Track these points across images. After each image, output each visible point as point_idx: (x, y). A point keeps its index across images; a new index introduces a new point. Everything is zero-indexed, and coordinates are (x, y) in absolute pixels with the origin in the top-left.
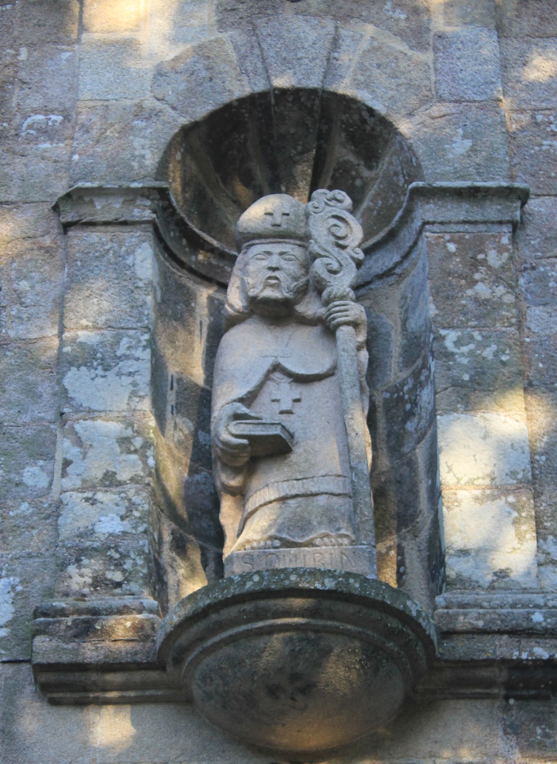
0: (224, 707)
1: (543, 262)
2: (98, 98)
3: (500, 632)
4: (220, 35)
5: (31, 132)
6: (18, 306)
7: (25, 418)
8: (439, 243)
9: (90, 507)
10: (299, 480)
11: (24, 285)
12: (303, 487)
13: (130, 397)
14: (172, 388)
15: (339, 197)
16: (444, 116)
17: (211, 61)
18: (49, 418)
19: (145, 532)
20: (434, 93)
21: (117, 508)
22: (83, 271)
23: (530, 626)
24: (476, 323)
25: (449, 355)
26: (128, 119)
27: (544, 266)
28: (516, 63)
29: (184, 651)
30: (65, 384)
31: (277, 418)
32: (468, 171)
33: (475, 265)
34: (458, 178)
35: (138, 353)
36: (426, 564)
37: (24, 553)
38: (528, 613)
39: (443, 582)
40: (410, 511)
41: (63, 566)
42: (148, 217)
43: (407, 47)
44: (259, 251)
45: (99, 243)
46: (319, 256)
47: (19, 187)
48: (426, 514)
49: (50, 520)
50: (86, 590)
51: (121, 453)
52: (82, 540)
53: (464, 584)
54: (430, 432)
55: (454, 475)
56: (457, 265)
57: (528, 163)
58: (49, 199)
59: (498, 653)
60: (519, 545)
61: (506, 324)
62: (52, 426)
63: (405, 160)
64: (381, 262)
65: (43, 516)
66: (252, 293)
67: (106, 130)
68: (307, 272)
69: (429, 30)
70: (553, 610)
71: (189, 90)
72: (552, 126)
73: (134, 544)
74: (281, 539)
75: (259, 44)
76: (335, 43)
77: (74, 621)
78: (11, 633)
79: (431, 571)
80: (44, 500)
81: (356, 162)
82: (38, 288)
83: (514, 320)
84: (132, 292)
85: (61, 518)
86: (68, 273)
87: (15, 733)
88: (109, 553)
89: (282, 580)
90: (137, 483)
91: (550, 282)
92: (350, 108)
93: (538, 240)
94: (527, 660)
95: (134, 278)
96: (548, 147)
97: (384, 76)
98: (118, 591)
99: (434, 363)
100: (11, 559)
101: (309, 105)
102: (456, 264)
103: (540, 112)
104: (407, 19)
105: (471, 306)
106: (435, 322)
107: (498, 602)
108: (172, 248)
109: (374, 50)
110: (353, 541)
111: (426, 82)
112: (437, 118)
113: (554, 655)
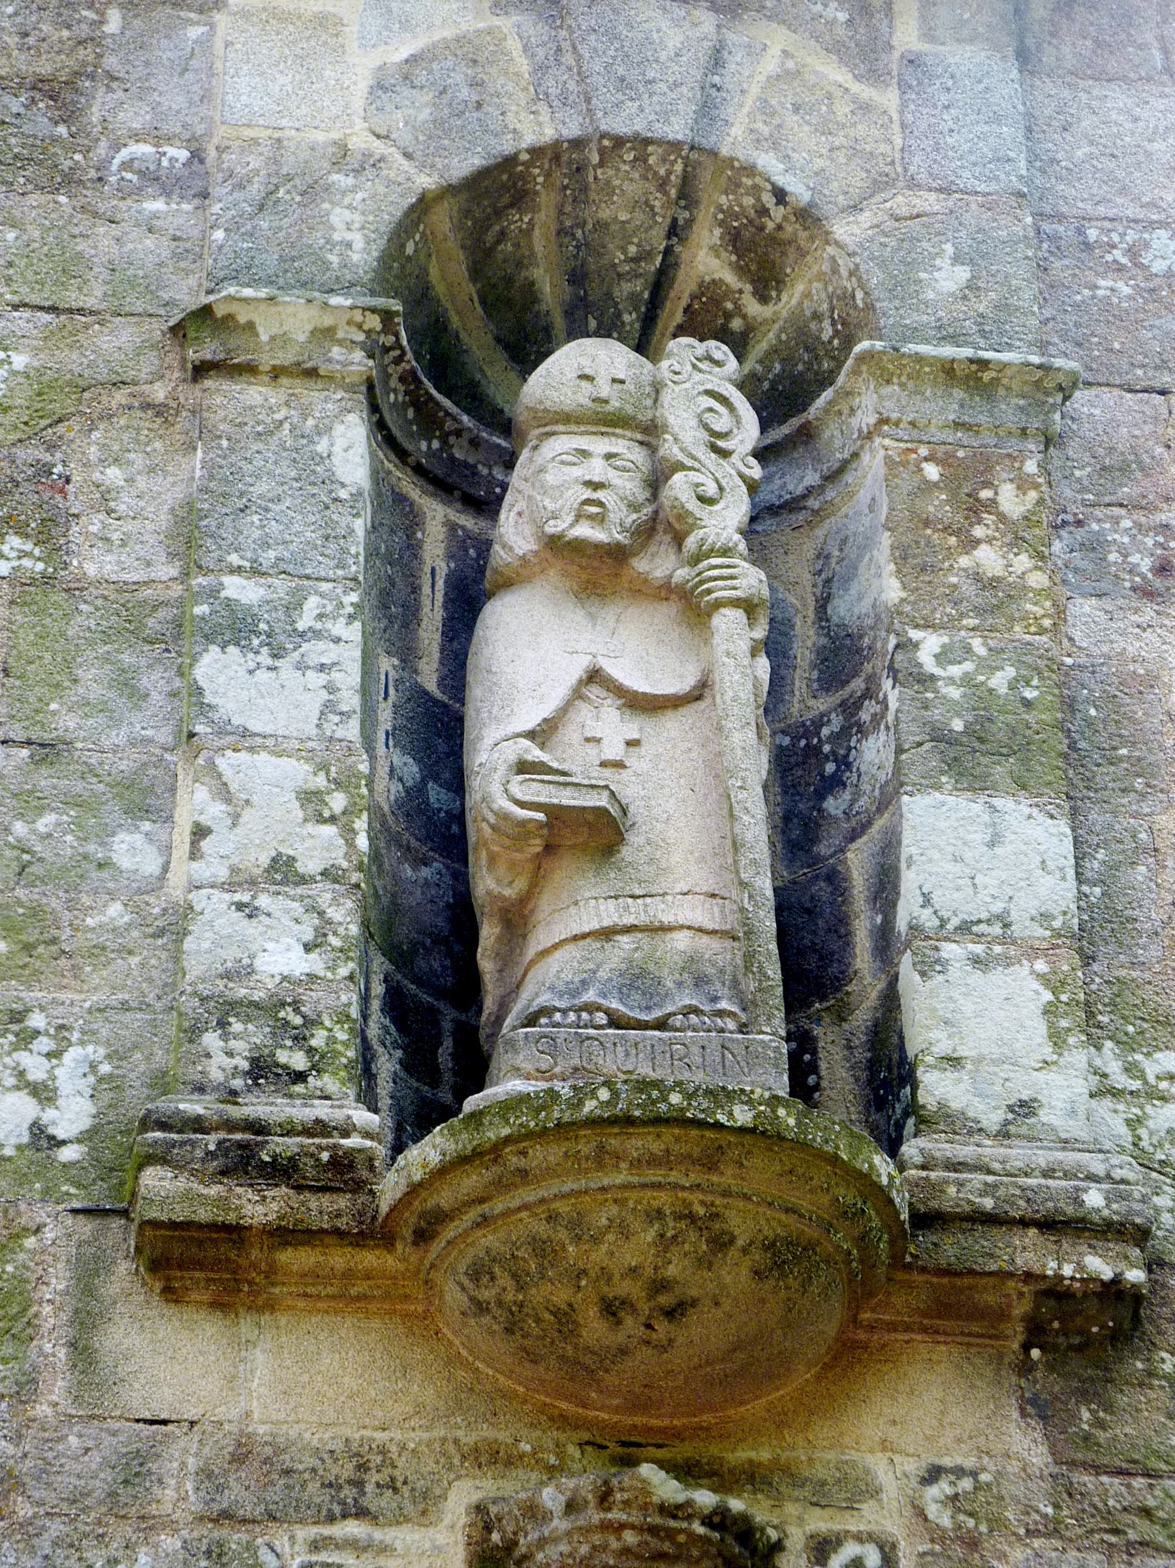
0: (508, 1331)
1: (1098, 512)
2: (261, 122)
3: (1024, 1223)
4: (497, 21)
5: (128, 176)
6: (102, 516)
7: (118, 737)
8: (908, 462)
9: (246, 922)
10: (639, 897)
11: (114, 475)
12: (646, 912)
13: (322, 713)
14: (385, 699)
15: (718, 355)
16: (918, 216)
17: (480, 69)
18: (163, 740)
19: (351, 977)
20: (899, 169)
21: (298, 926)
22: (233, 458)
23: (1080, 1215)
24: (977, 621)
25: (926, 680)
26: (320, 169)
27: (1099, 521)
28: (1049, 125)
29: (439, 1218)
30: (198, 678)
31: (595, 774)
32: (963, 327)
33: (975, 509)
34: (944, 338)
35: (338, 628)
36: (864, 1076)
37: (114, 1000)
38: (1077, 1189)
39: (906, 1114)
40: (833, 969)
41: (193, 1032)
42: (359, 364)
43: (850, 75)
44: (566, 448)
45: (262, 406)
46: (680, 467)
47: (106, 283)
48: (868, 980)
49: (165, 940)
50: (238, 1083)
51: (305, 820)
52: (231, 985)
53: (953, 1123)
54: (879, 823)
55: (935, 912)
56: (941, 506)
57: (1071, 319)
58: (162, 312)
59: (1019, 1261)
60: (1055, 1057)
61: (1033, 629)
62: (167, 756)
63: (839, 292)
64: (778, 482)
65: (150, 930)
66: (552, 528)
67: (277, 187)
68: (655, 496)
69: (892, 47)
70: (1122, 1187)
71: (438, 123)
72: (1115, 252)
73: (330, 1001)
74: (607, 1012)
75: (574, 48)
76: (717, 60)
77: (220, 1143)
78: (88, 1154)
79: (875, 1090)
80: (152, 900)
81: (739, 285)
82: (142, 483)
83: (1047, 623)
84: (327, 508)
85: (189, 939)
86: (203, 461)
87: (96, 1351)
88: (282, 1014)
89: (654, 1102)
90: (335, 881)
91: (1110, 552)
92: (738, 185)
93: (1089, 469)
94: (1072, 1278)
95: (330, 480)
96: (1108, 293)
97: (806, 128)
98: (299, 1088)
99: (896, 691)
100: (90, 1011)
101: (662, 172)
102: (938, 505)
103: (1094, 223)
104: (850, 22)
105: (968, 589)
106: (900, 613)
107: (1019, 1164)
108: (390, 424)
109: (787, 76)
110: (745, 1025)
111: (883, 148)
112: (906, 219)
113: (1121, 1274)
